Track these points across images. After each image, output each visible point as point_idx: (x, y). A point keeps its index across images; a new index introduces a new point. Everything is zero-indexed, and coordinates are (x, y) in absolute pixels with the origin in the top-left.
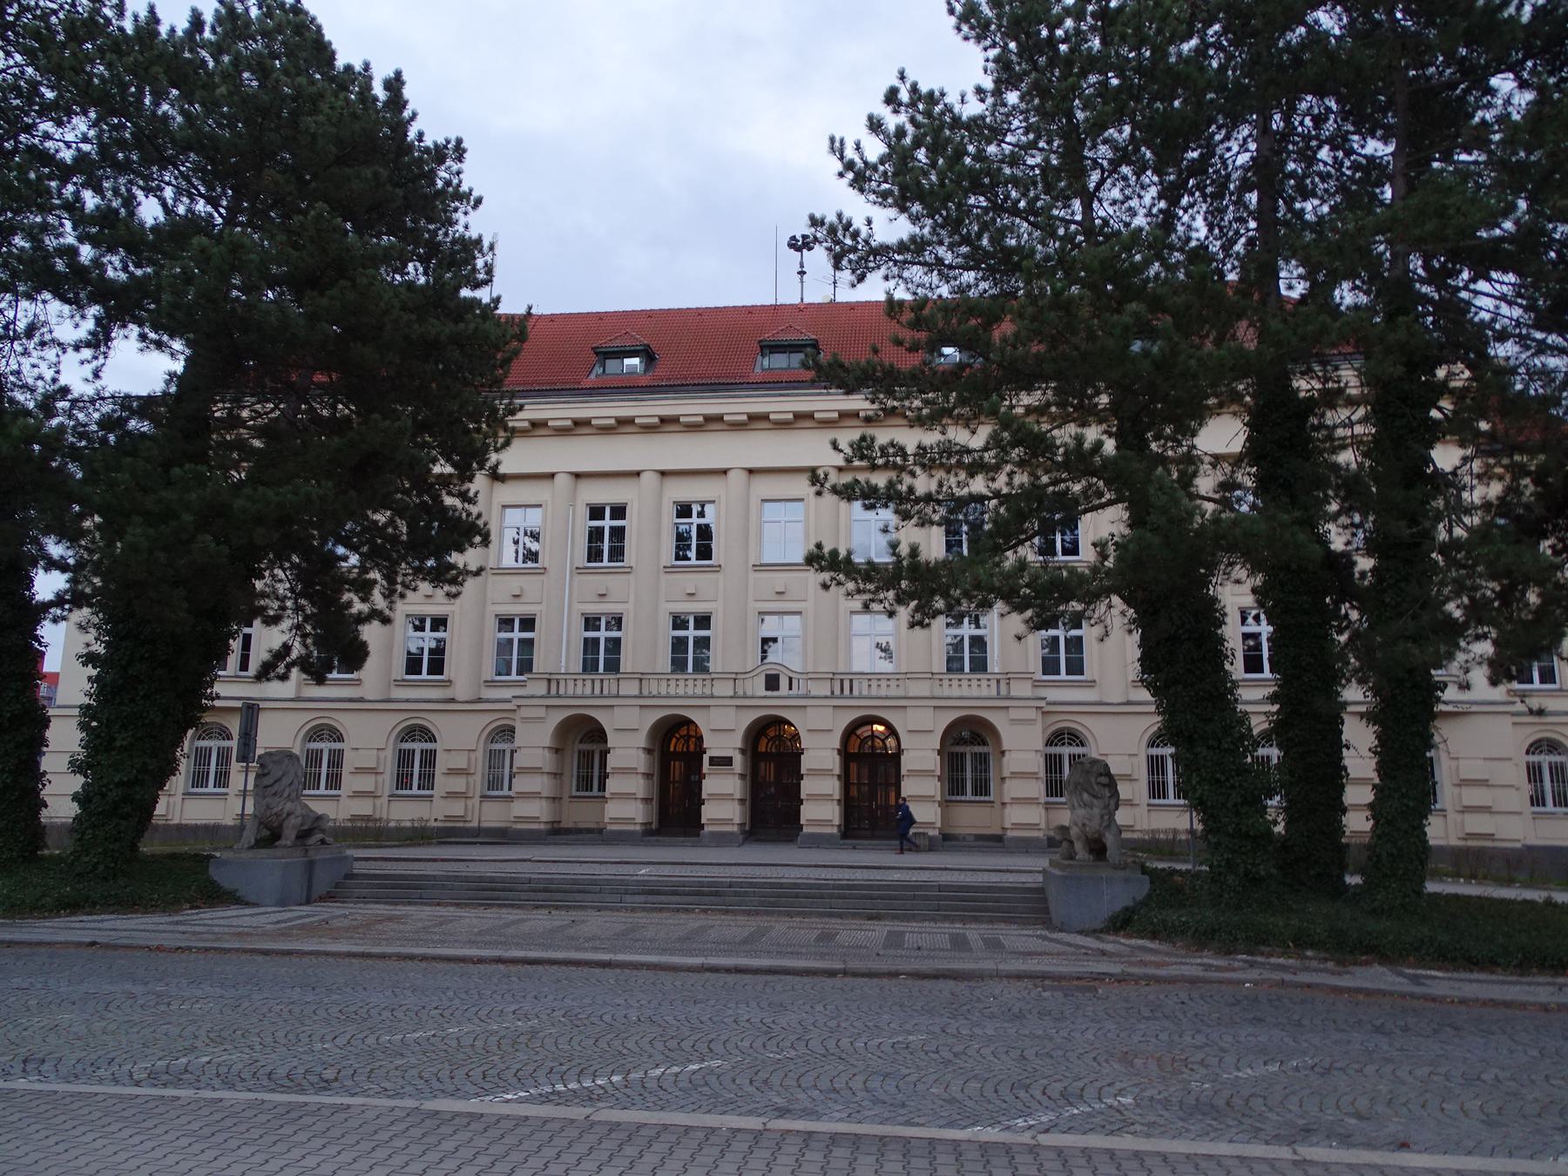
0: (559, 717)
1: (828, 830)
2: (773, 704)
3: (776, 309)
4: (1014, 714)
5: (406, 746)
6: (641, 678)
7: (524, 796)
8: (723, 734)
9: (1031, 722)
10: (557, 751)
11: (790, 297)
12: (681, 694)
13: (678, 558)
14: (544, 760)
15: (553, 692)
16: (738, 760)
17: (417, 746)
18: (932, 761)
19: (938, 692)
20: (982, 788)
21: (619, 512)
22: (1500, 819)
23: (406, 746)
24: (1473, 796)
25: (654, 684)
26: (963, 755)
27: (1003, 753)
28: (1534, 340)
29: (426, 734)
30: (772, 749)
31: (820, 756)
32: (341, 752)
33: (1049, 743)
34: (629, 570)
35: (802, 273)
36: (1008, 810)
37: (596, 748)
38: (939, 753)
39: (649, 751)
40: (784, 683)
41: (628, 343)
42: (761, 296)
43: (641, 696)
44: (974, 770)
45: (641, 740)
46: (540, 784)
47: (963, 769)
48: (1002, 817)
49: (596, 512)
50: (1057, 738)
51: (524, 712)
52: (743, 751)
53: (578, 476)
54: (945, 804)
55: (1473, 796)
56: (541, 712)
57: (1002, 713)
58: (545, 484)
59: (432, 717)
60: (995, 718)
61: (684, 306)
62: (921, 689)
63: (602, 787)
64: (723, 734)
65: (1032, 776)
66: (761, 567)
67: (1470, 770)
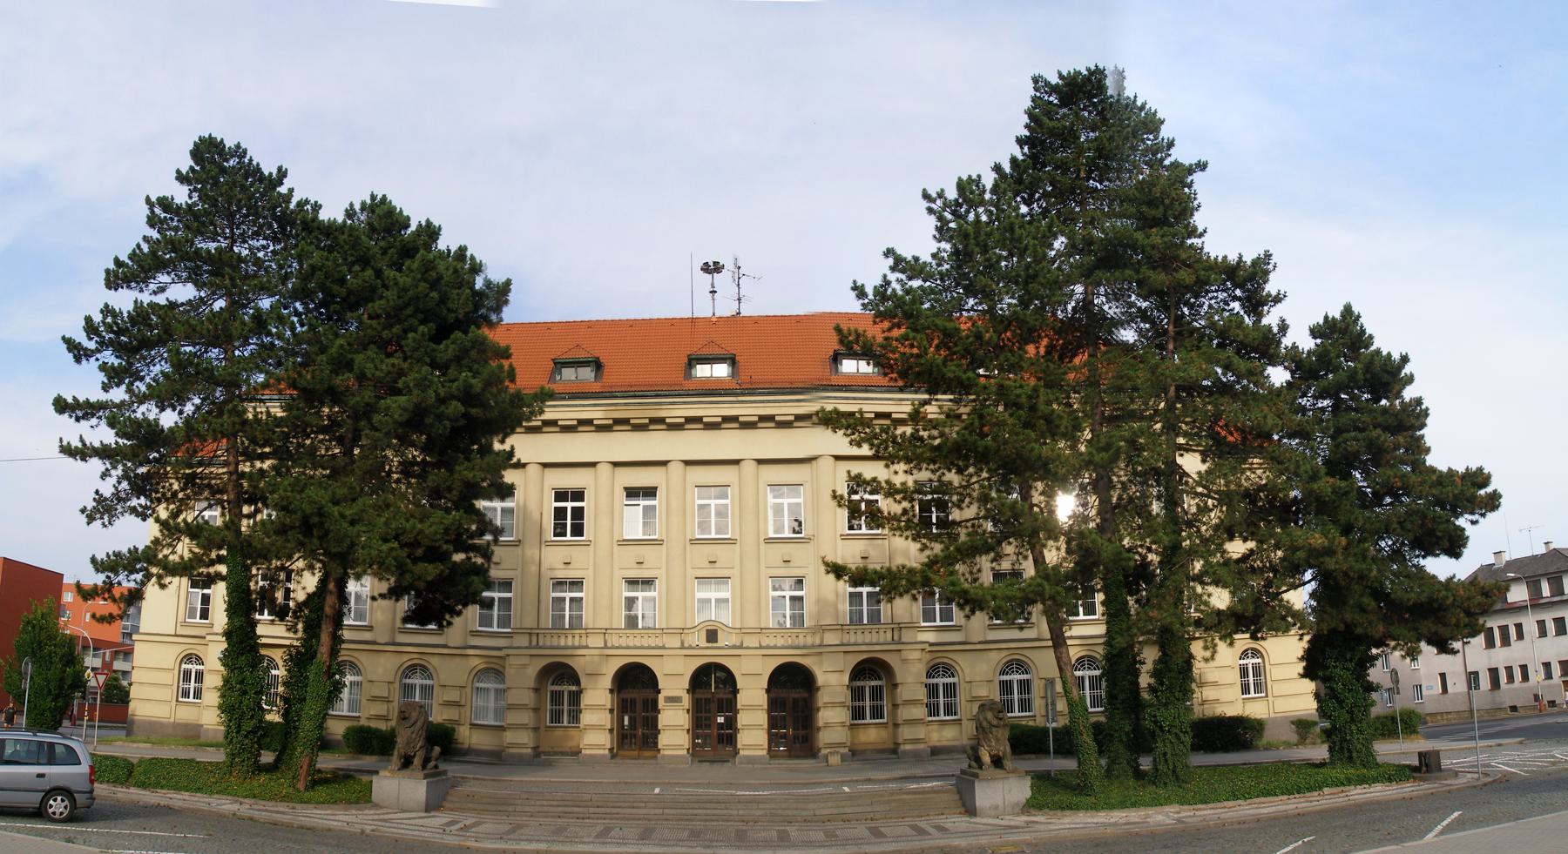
1: (601, 752)
5: (1005, 678)
8: (674, 679)
10: (536, 690)
11: (703, 310)
12: (631, 648)
13: (851, 528)
21: (578, 495)
23: (1005, 678)
27: (895, 686)
29: (948, 670)
31: (753, 698)
33: (929, 675)
34: (587, 544)
35: (713, 292)
36: (901, 729)
37: (567, 688)
39: (611, 691)
41: (716, 351)
44: (1020, 692)
46: (525, 718)
49: (561, 495)
50: (933, 671)
53: (545, 465)
56: (526, 661)
58: (659, 470)
61: (594, 318)
62: (831, 638)
64: (674, 679)
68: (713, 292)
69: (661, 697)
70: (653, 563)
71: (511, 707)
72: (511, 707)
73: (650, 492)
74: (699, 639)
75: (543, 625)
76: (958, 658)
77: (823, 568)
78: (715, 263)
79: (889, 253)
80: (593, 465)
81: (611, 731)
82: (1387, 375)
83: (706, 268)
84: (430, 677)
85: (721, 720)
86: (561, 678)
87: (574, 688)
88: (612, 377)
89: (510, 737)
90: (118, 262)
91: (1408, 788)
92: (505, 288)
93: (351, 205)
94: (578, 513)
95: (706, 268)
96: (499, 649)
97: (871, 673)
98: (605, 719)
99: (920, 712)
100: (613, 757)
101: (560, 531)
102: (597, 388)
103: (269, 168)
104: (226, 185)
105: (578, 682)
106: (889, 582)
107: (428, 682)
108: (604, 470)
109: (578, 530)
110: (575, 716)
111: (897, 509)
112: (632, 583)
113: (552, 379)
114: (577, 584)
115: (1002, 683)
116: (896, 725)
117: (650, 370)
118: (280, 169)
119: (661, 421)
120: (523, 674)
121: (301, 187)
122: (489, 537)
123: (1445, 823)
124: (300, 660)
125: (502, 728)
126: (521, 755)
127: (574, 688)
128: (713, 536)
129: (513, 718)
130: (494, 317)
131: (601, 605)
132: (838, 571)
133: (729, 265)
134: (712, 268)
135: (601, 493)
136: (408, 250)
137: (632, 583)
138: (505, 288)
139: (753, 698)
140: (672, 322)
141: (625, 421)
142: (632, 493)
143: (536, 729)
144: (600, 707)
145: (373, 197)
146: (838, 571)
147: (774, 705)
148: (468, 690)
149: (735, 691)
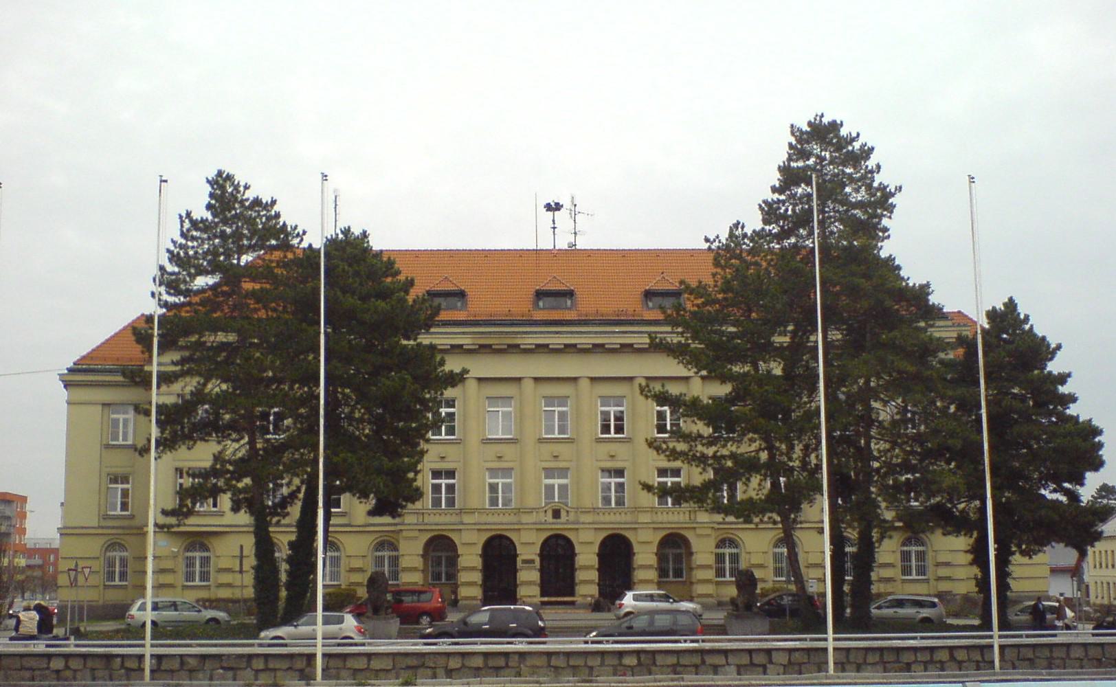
0: (426, 537)
2: (558, 526)
3: (537, 252)
5: (109, 554)
8: (528, 548)
9: (708, 535)
11: (546, 244)
14: (418, 562)
16: (538, 559)
17: (727, 551)
18: (652, 560)
19: (655, 519)
20: (678, 573)
22: (957, 584)
24: (943, 572)
26: (194, 558)
28: (251, 248)
29: (732, 543)
30: (499, 554)
32: (208, 558)
33: (718, 546)
36: (695, 586)
38: (423, 556)
40: (563, 514)
42: (525, 242)
44: (917, 560)
47: (668, 562)
48: (690, 591)
50: (722, 543)
51: (404, 534)
55: (943, 572)
56: (416, 534)
60: (689, 535)
63: (689, 575)
64: (528, 548)
65: (709, 567)
66: (541, 441)
67: (942, 558)
69: (518, 559)
74: (549, 518)
76: (740, 534)
78: (557, 204)
82: (1040, 351)
83: (549, 207)
84: (338, 549)
95: (549, 207)
97: (674, 547)
99: (710, 574)
103: (266, 199)
106: (680, 495)
107: (336, 554)
114: (451, 474)
115: (717, 555)
116: (692, 583)
117: (553, 299)
119: (517, 346)
121: (289, 215)
123: (321, 504)
131: (475, 487)
132: (648, 487)
133: (566, 203)
134: (554, 208)
136: (384, 295)
146: (648, 487)
147: (661, 557)
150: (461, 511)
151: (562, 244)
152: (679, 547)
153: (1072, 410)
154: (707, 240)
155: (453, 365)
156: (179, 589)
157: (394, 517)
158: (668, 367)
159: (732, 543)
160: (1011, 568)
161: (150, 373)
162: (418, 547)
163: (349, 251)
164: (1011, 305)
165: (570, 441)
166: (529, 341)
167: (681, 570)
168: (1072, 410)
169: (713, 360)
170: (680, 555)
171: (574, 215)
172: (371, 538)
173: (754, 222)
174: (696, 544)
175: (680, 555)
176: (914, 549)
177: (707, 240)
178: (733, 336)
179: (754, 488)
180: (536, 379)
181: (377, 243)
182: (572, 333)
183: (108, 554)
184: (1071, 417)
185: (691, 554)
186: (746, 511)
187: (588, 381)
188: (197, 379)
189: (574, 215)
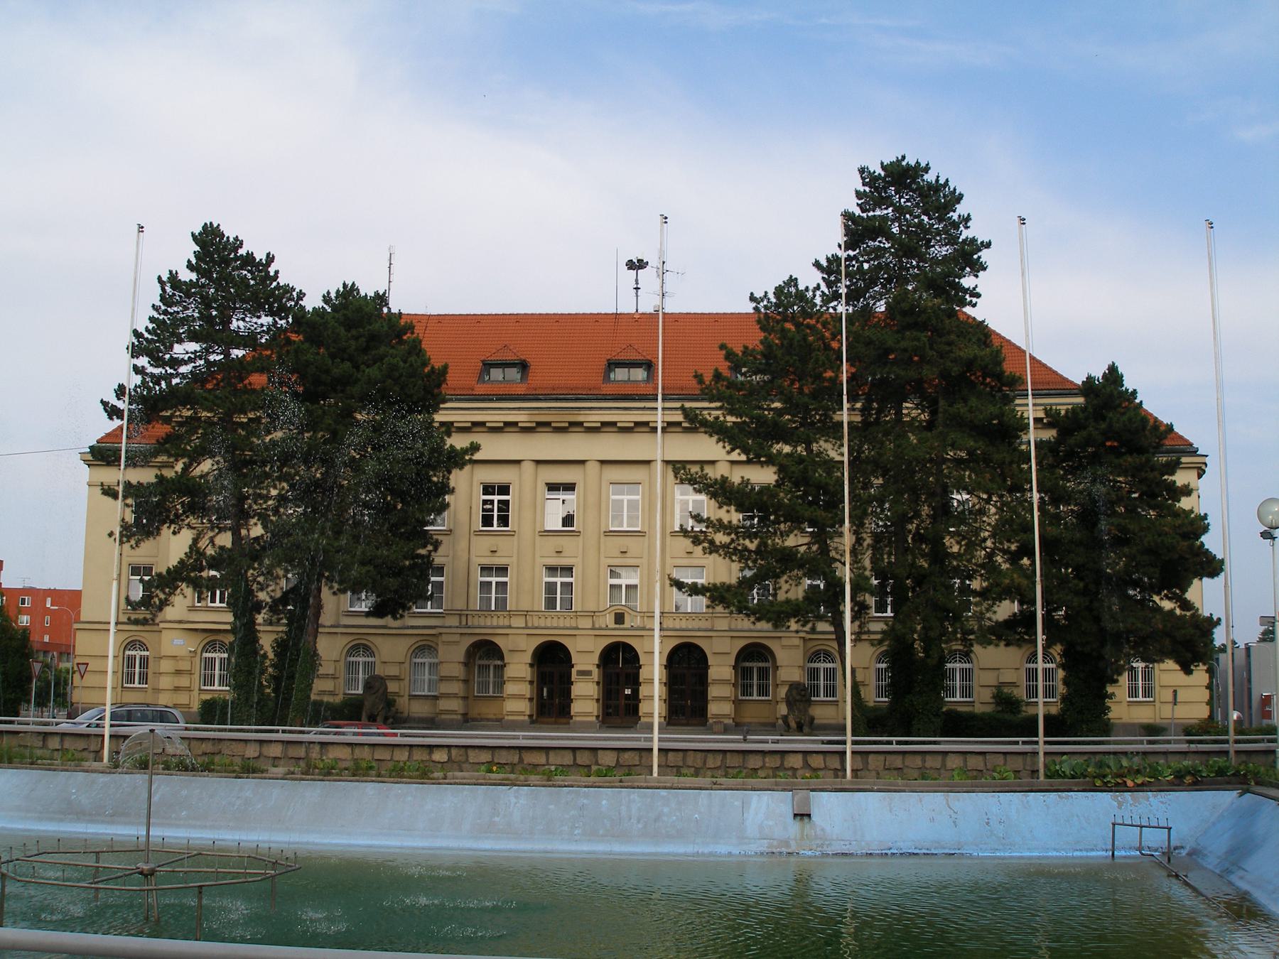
1: (521, 718)
2: (620, 635)
3: (617, 316)
4: (784, 642)
6: (526, 613)
7: (447, 696)
8: (585, 656)
11: (627, 307)
12: (553, 626)
15: (464, 623)
16: (595, 671)
19: (733, 627)
21: (504, 489)
25: (536, 619)
29: (367, 650)
30: (620, 663)
31: (654, 672)
34: (512, 534)
35: (637, 289)
38: (734, 668)
39: (531, 665)
42: (601, 303)
43: (527, 627)
45: (528, 658)
46: (456, 688)
47: (752, 678)
49: (488, 489)
50: (355, 649)
51: (444, 638)
52: (598, 666)
54: (737, 703)
56: (457, 638)
57: (776, 641)
59: (371, 638)
64: (585, 656)
66: (609, 533)
68: (637, 289)
69: (574, 671)
70: (572, 551)
71: (443, 679)
72: (443, 679)
73: (570, 487)
74: (610, 620)
75: (471, 607)
77: (668, 582)
79: (722, 347)
80: (518, 462)
81: (531, 699)
83: (631, 265)
84: (372, 654)
85: (628, 692)
86: (486, 653)
87: (499, 663)
88: (538, 378)
89: (444, 705)
90: (137, 334)
91: (140, 628)
92: (445, 368)
93: (328, 293)
94: (504, 505)
95: (631, 265)
96: (435, 627)
97: (754, 658)
98: (525, 689)
100: (532, 722)
101: (487, 521)
102: (521, 389)
103: (260, 256)
104: (223, 273)
105: (502, 657)
107: (370, 659)
108: (528, 468)
109: (504, 521)
110: (500, 684)
111: (726, 539)
112: (552, 570)
113: (480, 379)
116: (465, 698)
117: (576, 368)
118: (268, 254)
119: (580, 424)
120: (453, 656)
121: (288, 273)
122: (430, 548)
124: (282, 647)
125: (436, 698)
126: (452, 720)
127: (499, 663)
128: (625, 528)
129: (445, 688)
130: (436, 391)
131: (526, 587)
134: (637, 265)
135: (524, 485)
137: (552, 570)
138: (445, 368)
139: (654, 672)
140: (597, 318)
141: (548, 424)
142: (553, 487)
143: (465, 698)
144: (521, 680)
145: (345, 285)
148: (407, 665)
149: (707, 667)
150: (577, 615)
151: (647, 307)
152: (766, 660)
153: (1185, 503)
154: (752, 298)
155: (458, 442)
156: (1125, 704)
157: (395, 618)
158: (705, 448)
159: (367, 650)
160: (1205, 695)
161: (1038, 491)
162: (459, 653)
163: (358, 316)
164: (1113, 375)
165: (640, 534)
166: (594, 418)
167: (767, 686)
168: (1185, 503)
169: (751, 438)
170: (767, 669)
171: (662, 273)
172: (345, 640)
173: (810, 279)
174: (781, 655)
175: (767, 669)
176: (822, 665)
177: (752, 298)
178: (779, 412)
179: (793, 589)
180: (538, 462)
181: (396, 305)
182: (644, 408)
183: (127, 653)
184: (1188, 513)
185: (776, 668)
186: (778, 615)
187: (598, 464)
188: (185, 460)
189: (662, 273)
